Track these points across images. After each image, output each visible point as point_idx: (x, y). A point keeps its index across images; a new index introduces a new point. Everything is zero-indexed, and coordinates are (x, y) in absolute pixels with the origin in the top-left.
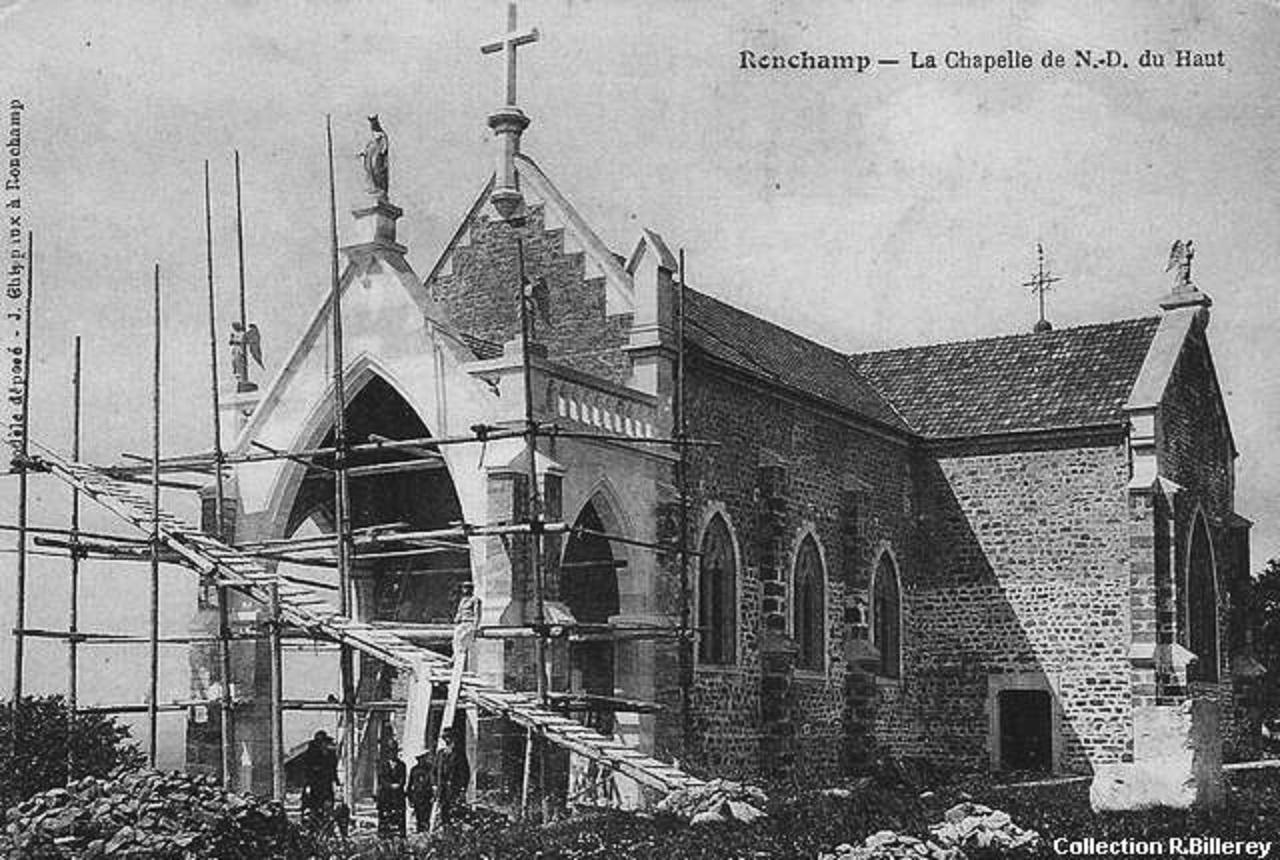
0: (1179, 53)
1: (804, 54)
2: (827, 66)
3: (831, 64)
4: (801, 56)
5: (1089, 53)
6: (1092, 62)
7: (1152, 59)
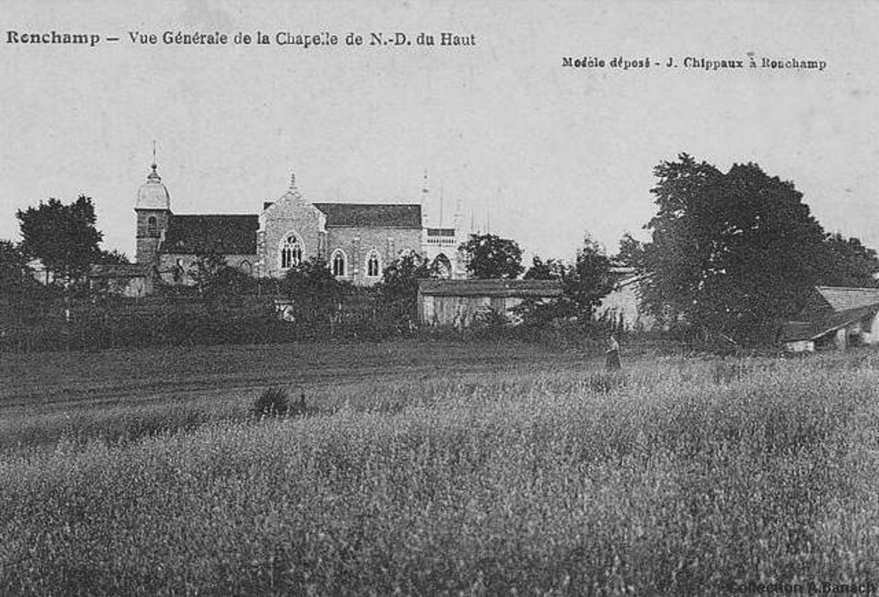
0: (443, 34)
1: (54, 33)
2: (69, 42)
3: (72, 39)
4: (51, 36)
5: (373, 44)
6: (382, 42)
7: (425, 39)
